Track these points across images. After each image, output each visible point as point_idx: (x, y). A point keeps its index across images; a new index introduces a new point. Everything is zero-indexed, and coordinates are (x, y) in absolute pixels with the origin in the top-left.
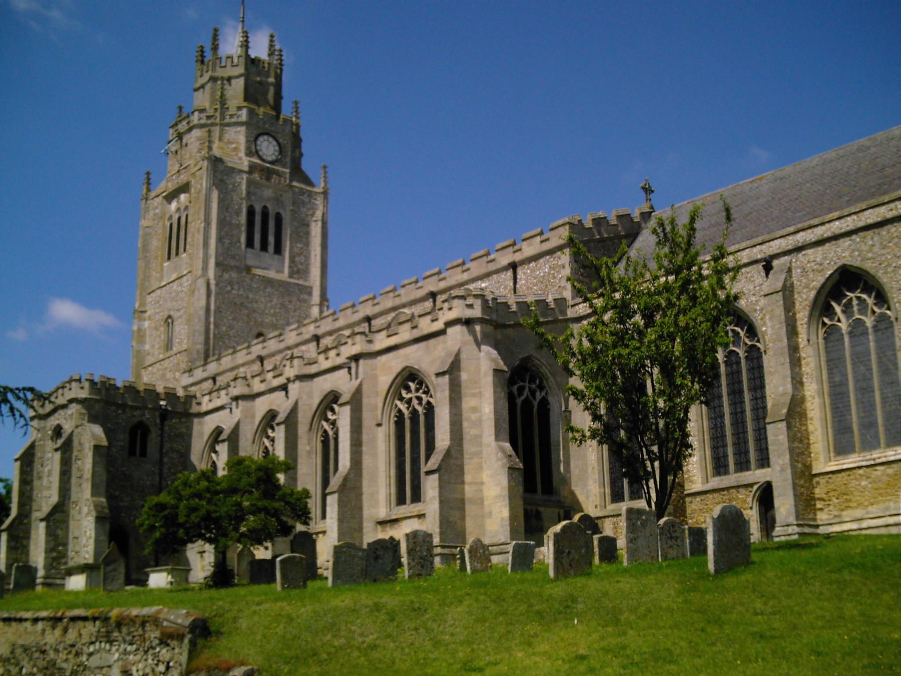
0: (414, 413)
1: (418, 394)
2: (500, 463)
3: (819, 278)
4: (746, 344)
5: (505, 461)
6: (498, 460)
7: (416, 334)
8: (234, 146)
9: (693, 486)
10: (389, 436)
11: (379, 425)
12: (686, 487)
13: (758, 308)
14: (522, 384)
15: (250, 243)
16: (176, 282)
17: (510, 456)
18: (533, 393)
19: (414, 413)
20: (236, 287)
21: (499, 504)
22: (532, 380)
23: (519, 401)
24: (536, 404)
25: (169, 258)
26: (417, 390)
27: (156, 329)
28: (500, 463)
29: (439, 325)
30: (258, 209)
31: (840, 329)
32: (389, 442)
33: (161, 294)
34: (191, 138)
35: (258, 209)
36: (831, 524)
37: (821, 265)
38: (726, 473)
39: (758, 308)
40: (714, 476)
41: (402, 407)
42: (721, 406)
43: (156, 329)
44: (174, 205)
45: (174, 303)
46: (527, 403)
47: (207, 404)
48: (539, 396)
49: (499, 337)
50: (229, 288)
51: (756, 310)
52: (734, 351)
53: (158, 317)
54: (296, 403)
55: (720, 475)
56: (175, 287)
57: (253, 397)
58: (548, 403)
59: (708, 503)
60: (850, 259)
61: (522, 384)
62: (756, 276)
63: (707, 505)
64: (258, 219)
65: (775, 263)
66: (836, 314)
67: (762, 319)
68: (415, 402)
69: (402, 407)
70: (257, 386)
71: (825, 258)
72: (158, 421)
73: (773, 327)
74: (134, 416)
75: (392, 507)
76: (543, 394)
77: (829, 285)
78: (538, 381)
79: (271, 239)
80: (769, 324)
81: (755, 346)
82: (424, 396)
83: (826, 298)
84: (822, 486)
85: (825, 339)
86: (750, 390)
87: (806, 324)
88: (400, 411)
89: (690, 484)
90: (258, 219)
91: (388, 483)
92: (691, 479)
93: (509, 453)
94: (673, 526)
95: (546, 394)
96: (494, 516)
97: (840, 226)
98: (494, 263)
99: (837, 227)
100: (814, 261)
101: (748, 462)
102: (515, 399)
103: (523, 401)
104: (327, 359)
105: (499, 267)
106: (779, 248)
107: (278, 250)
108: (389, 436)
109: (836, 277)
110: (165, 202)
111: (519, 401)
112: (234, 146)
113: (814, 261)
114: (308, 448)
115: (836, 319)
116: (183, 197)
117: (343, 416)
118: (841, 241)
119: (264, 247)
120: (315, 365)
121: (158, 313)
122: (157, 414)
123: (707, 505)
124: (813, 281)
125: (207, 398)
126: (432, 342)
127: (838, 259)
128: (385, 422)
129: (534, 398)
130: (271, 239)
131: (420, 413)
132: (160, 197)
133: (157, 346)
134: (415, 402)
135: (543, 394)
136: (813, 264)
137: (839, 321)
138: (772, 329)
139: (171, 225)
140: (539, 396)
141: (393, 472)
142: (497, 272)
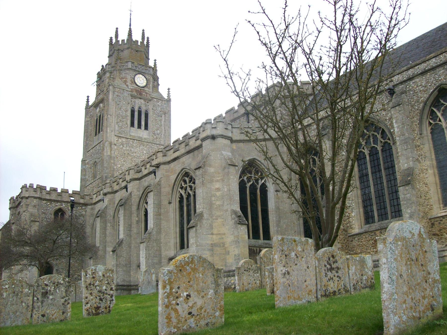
0: (189, 195)
1: (190, 184)
2: (233, 221)
3: (425, 95)
4: (381, 142)
5: (236, 219)
6: (232, 219)
7: (188, 148)
8: (124, 80)
9: (353, 231)
10: (176, 209)
11: (170, 203)
12: (349, 232)
13: (387, 118)
14: (250, 175)
15: (132, 125)
16: (98, 146)
17: (239, 216)
18: (257, 181)
19: (189, 195)
20: (125, 146)
21: (233, 246)
22: (257, 172)
23: (248, 185)
24: (259, 187)
25: (96, 135)
26: (190, 182)
27: (91, 168)
28: (233, 221)
29: (199, 142)
30: (136, 109)
31: (441, 125)
32: (176, 212)
33: (93, 151)
34: (105, 78)
35: (136, 109)
36: (444, 251)
37: (425, 87)
38: (373, 222)
39: (387, 118)
40: (365, 225)
41: (183, 192)
42: (368, 181)
43: (91, 168)
44: (98, 109)
45: (98, 155)
46: (253, 187)
47: (95, 199)
48: (261, 182)
49: (235, 148)
50: (121, 147)
51: (386, 120)
52: (374, 147)
53: (91, 162)
54: (131, 194)
55: (369, 224)
56: (98, 148)
57: (116, 192)
58: (266, 187)
59: (362, 241)
60: (444, 81)
61: (250, 175)
62: (384, 100)
63: (362, 242)
64: (136, 114)
65: (396, 89)
66: (438, 116)
67: (390, 125)
68: (188, 189)
69: (183, 192)
70: (116, 188)
71: (428, 82)
72: (70, 208)
73: (398, 127)
74: (56, 206)
75: (178, 250)
76: (263, 181)
77: (432, 98)
78: (259, 174)
79: (143, 123)
80: (395, 125)
81: (387, 142)
82: (193, 185)
83: (430, 107)
84: (436, 226)
85: (431, 133)
86: (385, 169)
87: (419, 124)
88: (181, 195)
89: (351, 230)
90: (136, 114)
91: (175, 236)
92: (352, 226)
93: (239, 215)
94: (333, 256)
95: (265, 181)
96: (230, 254)
97: (436, 61)
98: (237, 113)
99: (433, 62)
100: (421, 85)
101: (386, 214)
102: (245, 184)
103: (251, 185)
104: (146, 169)
105: (239, 115)
106: (398, 81)
107: (146, 128)
108: (176, 209)
109: (436, 92)
110: (94, 109)
111: (248, 185)
112: (124, 80)
113: (421, 85)
114: (137, 219)
115: (438, 119)
116: (101, 105)
117: (151, 199)
118: (438, 70)
119: (139, 127)
120: (141, 173)
121: (91, 161)
122: (69, 204)
123: (362, 242)
124: (421, 97)
125: (95, 195)
126: (196, 152)
127: (437, 82)
128: (173, 201)
129: (258, 184)
130: (143, 123)
131: (191, 195)
132: (93, 107)
133: (90, 176)
134: (188, 189)
135: (263, 181)
136: (420, 87)
137: (440, 121)
138: (398, 128)
139: (97, 119)
140: (261, 182)
141: (178, 230)
142: (238, 118)
